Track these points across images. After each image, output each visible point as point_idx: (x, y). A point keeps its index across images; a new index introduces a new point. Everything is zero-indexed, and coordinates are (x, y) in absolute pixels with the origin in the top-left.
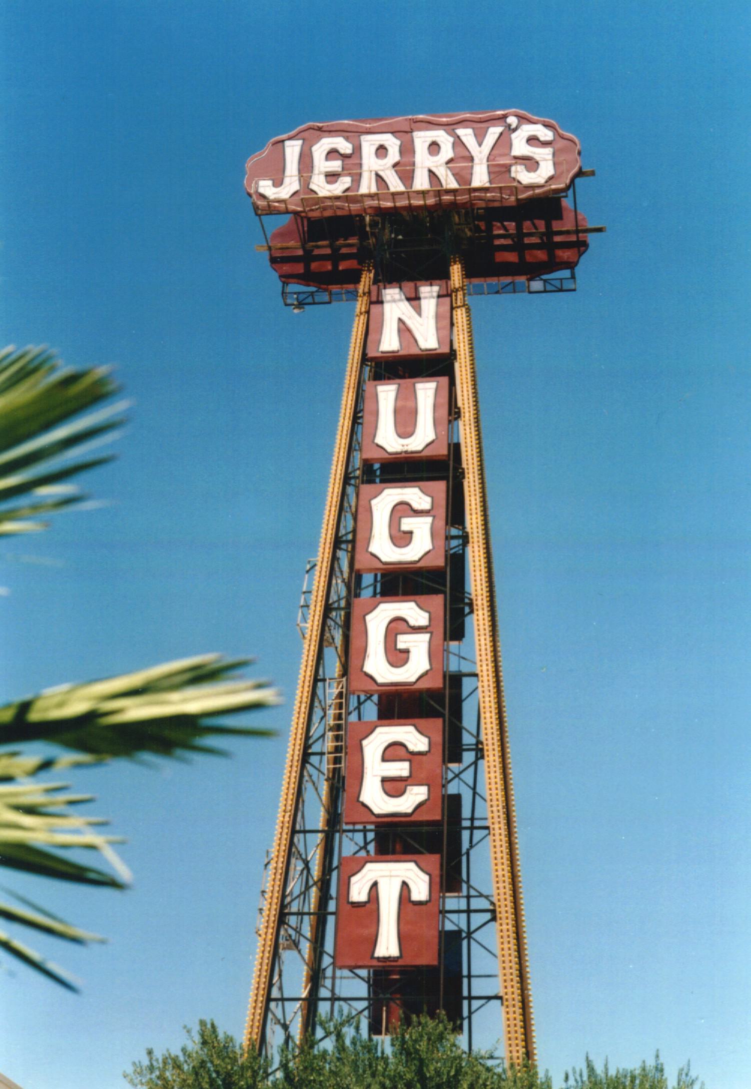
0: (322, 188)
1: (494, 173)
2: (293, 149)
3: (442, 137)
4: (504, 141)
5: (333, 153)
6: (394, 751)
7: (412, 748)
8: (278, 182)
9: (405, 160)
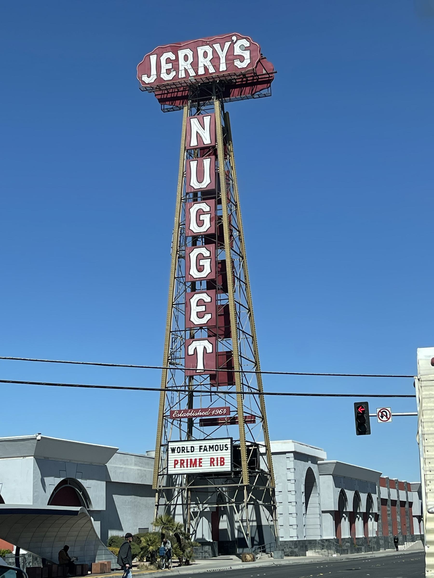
0: (165, 77)
1: (228, 63)
2: (153, 58)
3: (208, 48)
4: (231, 48)
6: (200, 303)
7: (172, 59)
8: (149, 77)
9: (198, 101)
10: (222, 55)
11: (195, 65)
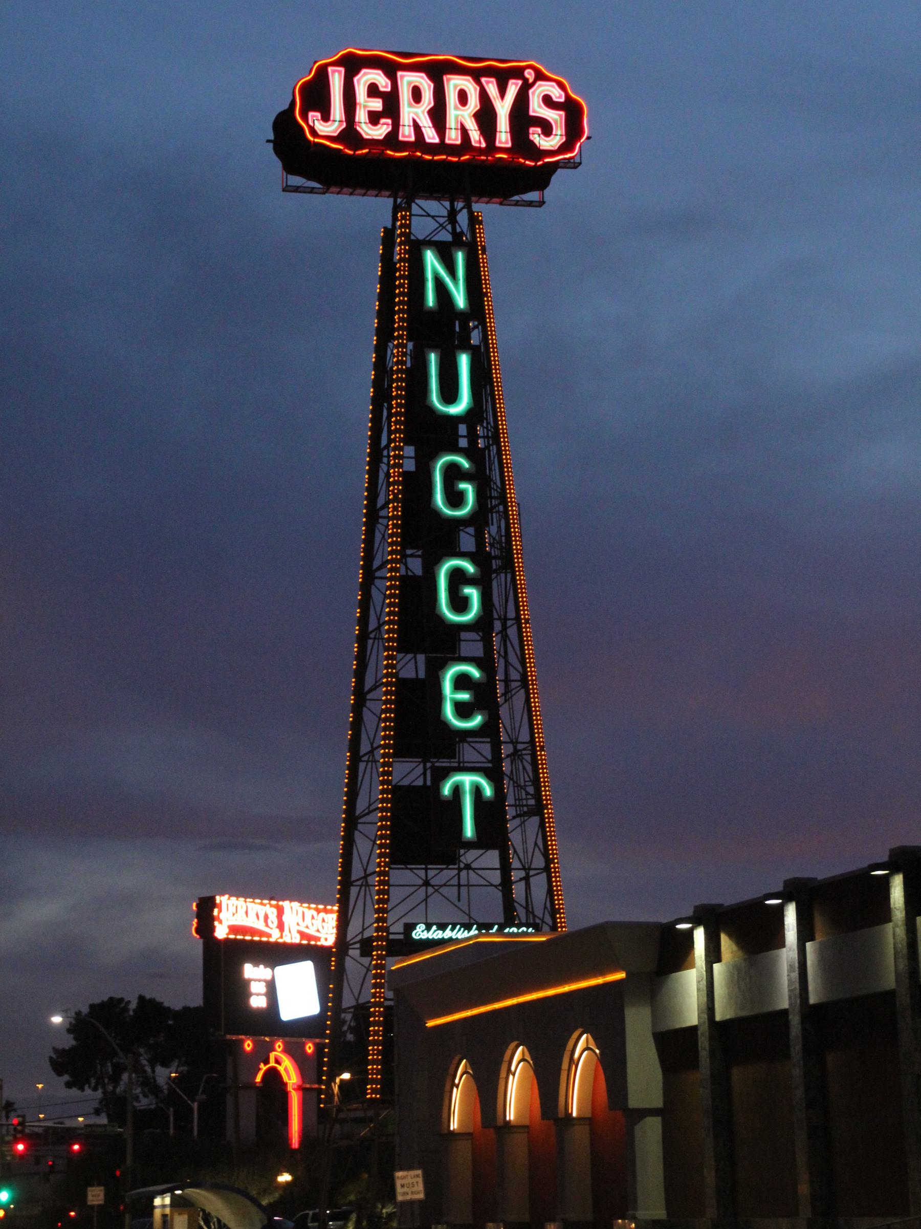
4: (522, 101)
5: (462, 682)
8: (326, 118)
10: (503, 108)
11: (438, 115)
